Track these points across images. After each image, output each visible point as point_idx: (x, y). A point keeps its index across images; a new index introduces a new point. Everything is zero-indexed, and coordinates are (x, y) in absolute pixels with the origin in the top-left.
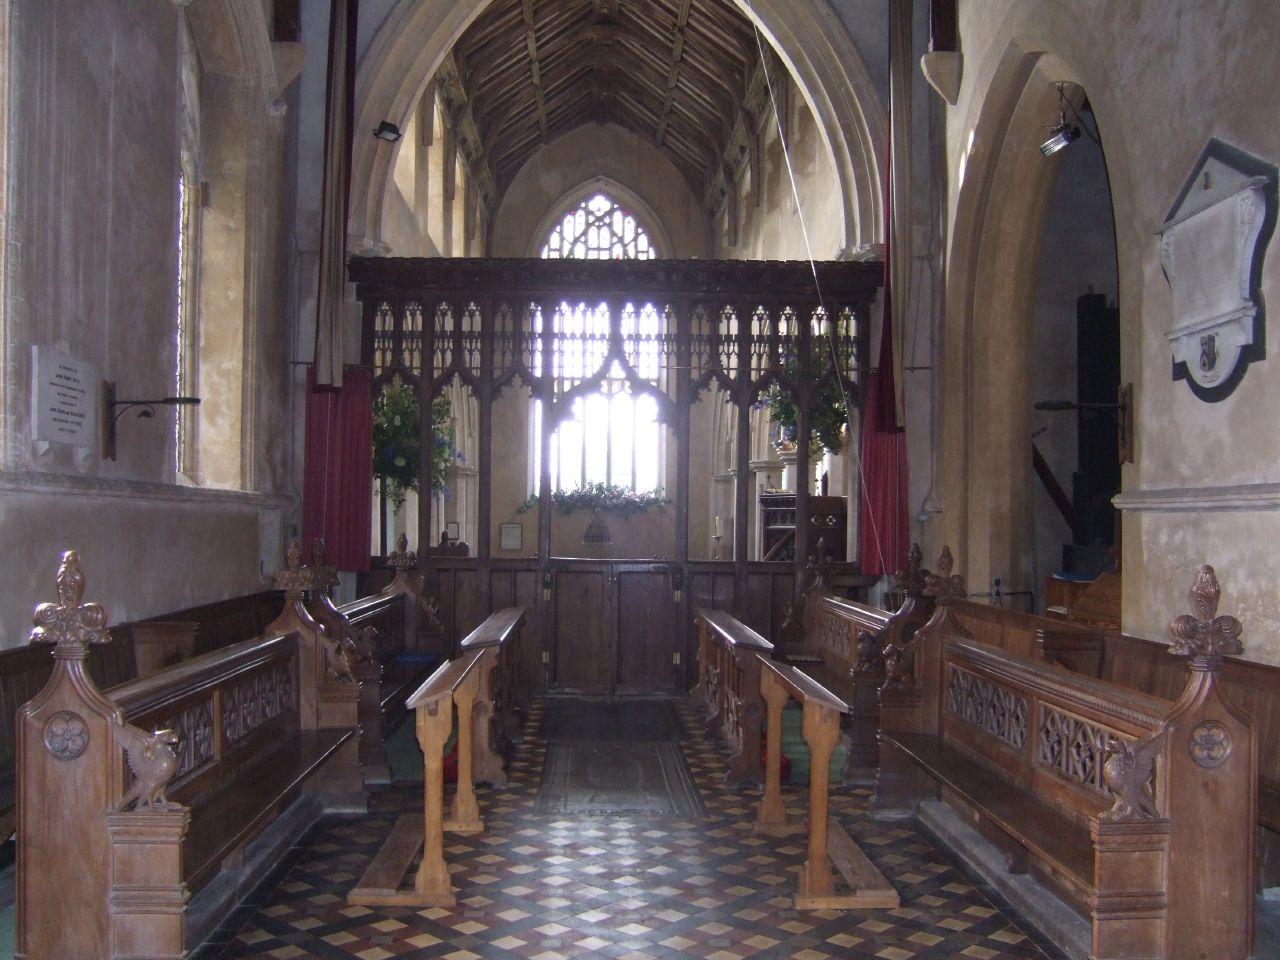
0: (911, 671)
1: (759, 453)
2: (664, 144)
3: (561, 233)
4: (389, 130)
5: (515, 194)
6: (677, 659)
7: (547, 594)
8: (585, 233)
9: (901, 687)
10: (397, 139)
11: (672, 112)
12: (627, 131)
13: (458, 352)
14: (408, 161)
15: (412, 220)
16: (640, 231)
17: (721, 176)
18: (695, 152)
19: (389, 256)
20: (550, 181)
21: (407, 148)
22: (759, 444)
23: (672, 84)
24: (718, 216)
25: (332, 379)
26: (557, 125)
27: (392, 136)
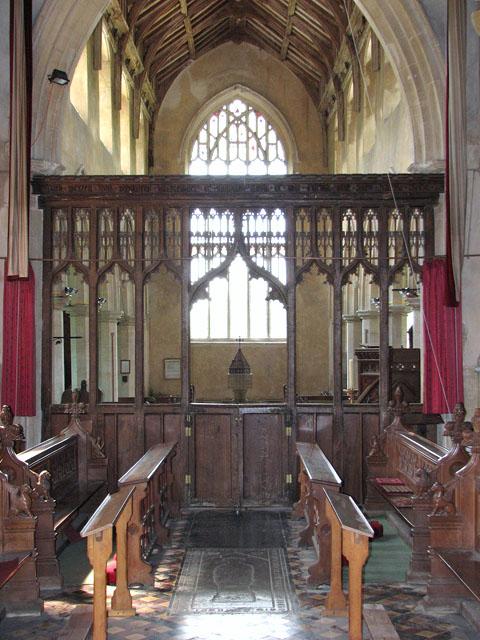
0: (452, 502)
1: (364, 305)
2: (287, 59)
3: (208, 130)
4: (61, 76)
5: (173, 98)
6: (289, 479)
7: (188, 431)
8: (226, 130)
9: (445, 514)
10: (66, 83)
11: (292, 33)
12: (258, 48)
13: (118, 248)
14: (82, 83)
15: (85, 131)
16: (270, 127)
17: (331, 86)
18: (311, 64)
19: (64, 173)
20: (198, 90)
21: (80, 75)
22: (364, 299)
23: (291, 12)
24: (330, 116)
25: (18, 271)
26: (202, 44)
27: (63, 81)
